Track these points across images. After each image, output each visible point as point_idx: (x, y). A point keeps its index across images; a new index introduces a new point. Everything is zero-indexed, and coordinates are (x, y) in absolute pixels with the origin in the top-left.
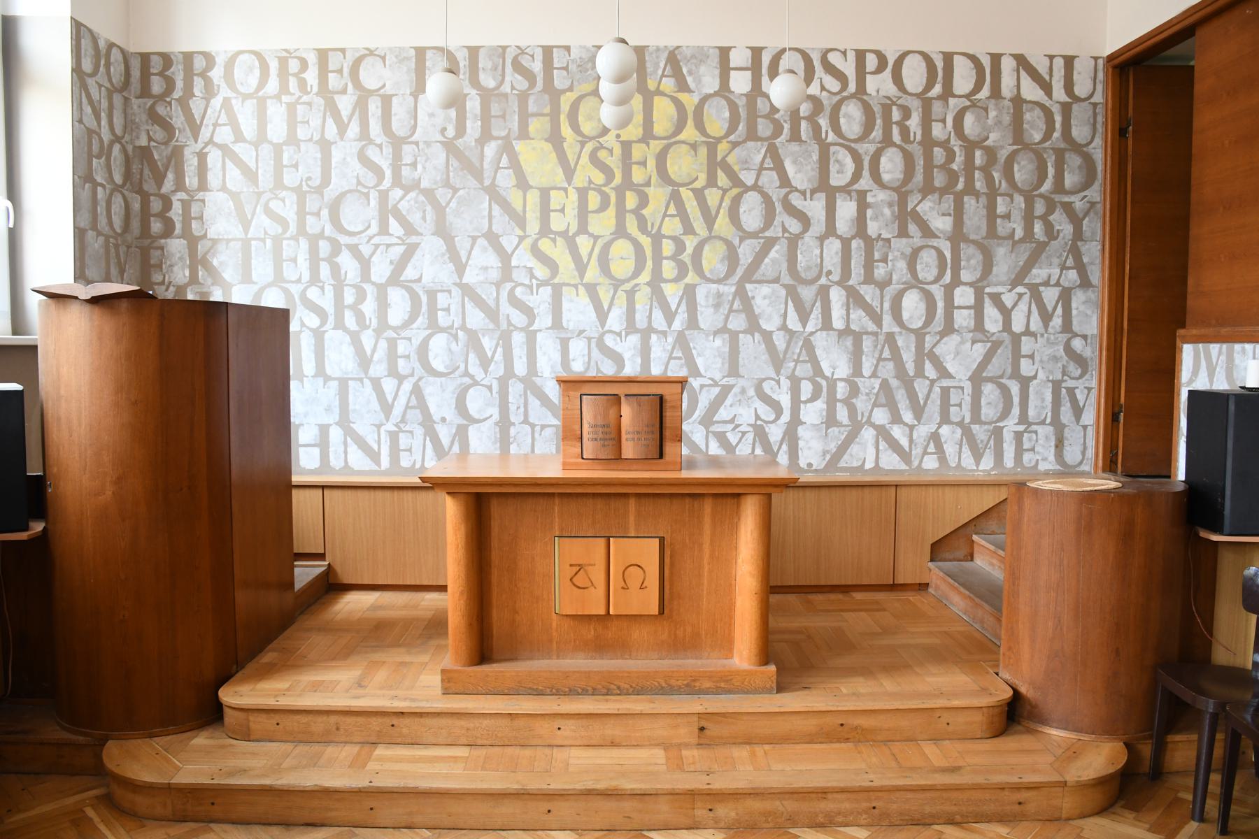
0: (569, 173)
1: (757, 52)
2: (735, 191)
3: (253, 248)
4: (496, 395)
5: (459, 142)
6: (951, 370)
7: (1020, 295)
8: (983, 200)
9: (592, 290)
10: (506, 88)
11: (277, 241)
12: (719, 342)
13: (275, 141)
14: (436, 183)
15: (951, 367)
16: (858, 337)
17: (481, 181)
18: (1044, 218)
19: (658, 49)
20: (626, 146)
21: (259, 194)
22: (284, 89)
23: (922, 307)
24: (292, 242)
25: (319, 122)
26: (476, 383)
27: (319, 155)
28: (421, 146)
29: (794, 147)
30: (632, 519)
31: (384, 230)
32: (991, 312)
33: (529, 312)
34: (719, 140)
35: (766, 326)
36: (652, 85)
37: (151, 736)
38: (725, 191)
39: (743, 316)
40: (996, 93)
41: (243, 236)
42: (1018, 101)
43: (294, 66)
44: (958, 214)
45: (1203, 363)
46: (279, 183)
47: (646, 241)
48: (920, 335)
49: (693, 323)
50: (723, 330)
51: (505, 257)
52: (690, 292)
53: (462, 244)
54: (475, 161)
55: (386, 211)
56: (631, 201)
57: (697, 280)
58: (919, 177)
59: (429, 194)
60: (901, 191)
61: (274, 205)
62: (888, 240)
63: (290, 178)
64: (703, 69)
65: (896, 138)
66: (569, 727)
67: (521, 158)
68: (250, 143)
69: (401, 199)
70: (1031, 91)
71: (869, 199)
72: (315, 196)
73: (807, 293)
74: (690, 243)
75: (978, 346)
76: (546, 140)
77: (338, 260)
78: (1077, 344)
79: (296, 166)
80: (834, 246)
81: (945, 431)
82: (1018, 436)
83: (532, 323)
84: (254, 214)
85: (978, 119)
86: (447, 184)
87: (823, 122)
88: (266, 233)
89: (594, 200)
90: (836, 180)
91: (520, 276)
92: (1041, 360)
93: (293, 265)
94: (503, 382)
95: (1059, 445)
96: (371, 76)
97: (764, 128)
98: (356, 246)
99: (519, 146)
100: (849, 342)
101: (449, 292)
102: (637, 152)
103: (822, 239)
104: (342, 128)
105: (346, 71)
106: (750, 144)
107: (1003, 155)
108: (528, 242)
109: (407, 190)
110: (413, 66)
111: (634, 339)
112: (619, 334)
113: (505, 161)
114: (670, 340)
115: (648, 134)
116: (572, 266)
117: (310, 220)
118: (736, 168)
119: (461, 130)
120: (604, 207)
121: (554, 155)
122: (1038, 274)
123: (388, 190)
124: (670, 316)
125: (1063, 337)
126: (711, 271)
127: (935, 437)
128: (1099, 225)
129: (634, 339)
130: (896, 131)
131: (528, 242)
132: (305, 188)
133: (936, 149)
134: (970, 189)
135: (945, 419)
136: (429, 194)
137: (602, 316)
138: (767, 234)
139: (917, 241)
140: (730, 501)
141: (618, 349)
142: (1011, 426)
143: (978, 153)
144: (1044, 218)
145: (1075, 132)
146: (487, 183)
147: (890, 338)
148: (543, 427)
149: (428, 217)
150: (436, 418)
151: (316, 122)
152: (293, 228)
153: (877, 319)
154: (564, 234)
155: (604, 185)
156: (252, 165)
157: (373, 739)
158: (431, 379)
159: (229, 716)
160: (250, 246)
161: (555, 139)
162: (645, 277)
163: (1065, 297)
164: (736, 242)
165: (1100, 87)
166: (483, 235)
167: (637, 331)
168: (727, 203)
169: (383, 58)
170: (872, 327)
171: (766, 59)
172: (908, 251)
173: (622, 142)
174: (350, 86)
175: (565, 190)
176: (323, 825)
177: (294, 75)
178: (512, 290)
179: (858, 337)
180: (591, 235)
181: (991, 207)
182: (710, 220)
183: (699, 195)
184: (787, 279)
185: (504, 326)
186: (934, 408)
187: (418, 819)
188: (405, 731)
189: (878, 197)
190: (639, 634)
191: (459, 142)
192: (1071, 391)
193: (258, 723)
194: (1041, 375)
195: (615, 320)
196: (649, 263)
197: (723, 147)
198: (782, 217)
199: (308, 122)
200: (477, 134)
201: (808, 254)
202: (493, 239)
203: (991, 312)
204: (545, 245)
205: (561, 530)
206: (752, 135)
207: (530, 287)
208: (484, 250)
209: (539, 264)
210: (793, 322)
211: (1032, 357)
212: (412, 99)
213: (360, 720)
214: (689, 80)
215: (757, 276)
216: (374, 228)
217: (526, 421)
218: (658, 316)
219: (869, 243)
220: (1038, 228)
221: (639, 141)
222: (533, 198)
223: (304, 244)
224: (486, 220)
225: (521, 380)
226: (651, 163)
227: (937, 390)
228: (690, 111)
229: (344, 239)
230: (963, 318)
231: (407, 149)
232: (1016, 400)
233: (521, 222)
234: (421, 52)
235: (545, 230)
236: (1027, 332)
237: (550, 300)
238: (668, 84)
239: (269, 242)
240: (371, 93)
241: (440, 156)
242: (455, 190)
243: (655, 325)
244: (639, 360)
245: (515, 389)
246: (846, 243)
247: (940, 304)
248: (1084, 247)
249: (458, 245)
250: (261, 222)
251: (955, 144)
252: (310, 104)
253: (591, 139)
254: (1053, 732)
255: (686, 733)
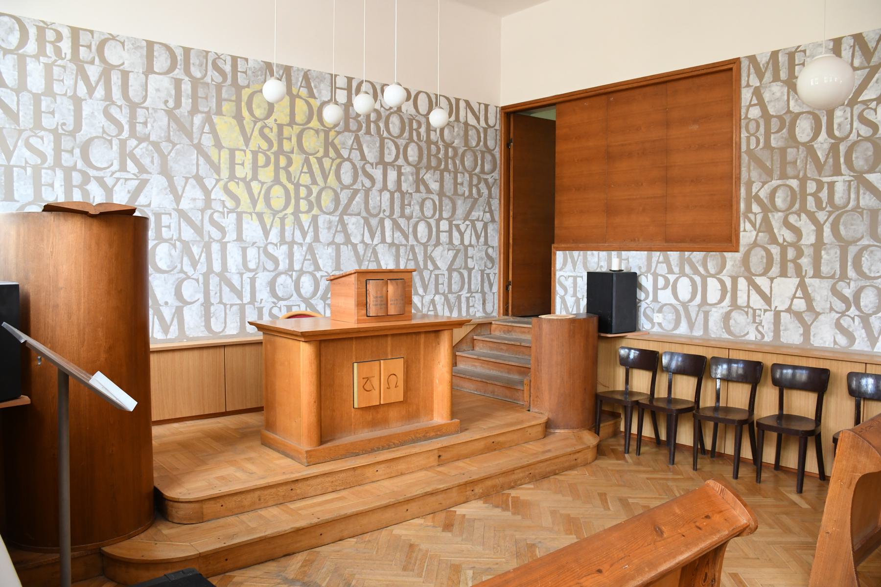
0: (247, 141)
1: (350, 80)
2: (338, 160)
3: (15, 174)
4: (201, 285)
5: (177, 112)
6: (439, 265)
7: (468, 225)
8: (452, 174)
9: (260, 216)
10: (208, 79)
11: (37, 170)
12: (330, 250)
13: (34, 91)
14: (160, 138)
15: (439, 264)
16: (398, 247)
17: (191, 139)
18: (477, 186)
19: (298, 70)
20: (280, 127)
21: (21, 132)
22: (42, 51)
23: (426, 230)
24: (49, 172)
25: (72, 82)
26: (188, 277)
27: (72, 107)
28: (150, 111)
29: (368, 137)
30: (389, 349)
31: (123, 168)
32: (456, 234)
33: (222, 230)
34: (330, 129)
35: (354, 241)
36: (295, 91)
37: (130, 537)
38: (333, 160)
39: (343, 234)
40: (457, 119)
41: (5, 163)
42: (466, 124)
43: (50, 35)
44: (442, 181)
45: (569, 260)
46: (38, 125)
47: (291, 187)
48: (425, 245)
49: (316, 239)
50: (332, 243)
51: (207, 192)
52: (315, 219)
53: (179, 182)
54: (188, 125)
55: (124, 155)
56: (283, 162)
57: (319, 212)
58: (425, 160)
59: (156, 145)
60: (417, 167)
61: (33, 141)
62: (411, 194)
63: (47, 122)
64: (322, 85)
65: (415, 138)
66: (382, 469)
67: (218, 128)
68: (12, 89)
69: (136, 147)
70: (472, 121)
71: (403, 171)
72: (69, 138)
73: (374, 222)
74: (315, 190)
75: (450, 252)
76: (234, 117)
77: (88, 187)
78: (490, 251)
79: (53, 113)
80: (386, 196)
81: (437, 298)
82: (468, 299)
83: (224, 237)
84: (15, 146)
85: (450, 132)
86: (168, 140)
87: (382, 125)
88: (26, 162)
89: (261, 159)
90: (388, 158)
91: (217, 206)
92: (476, 259)
93: (50, 189)
94: (206, 276)
95: (484, 304)
96: (113, 55)
97: (353, 126)
98: (102, 178)
99: (216, 119)
100: (394, 250)
101: (170, 214)
102: (287, 131)
103: (381, 191)
104: (91, 90)
105: (94, 48)
106: (346, 133)
107: (460, 151)
108: (222, 183)
109: (141, 140)
110: (145, 53)
111: (285, 248)
112: (276, 245)
113: (207, 128)
114: (305, 248)
115: (292, 122)
116: (249, 201)
117: (65, 156)
118: (339, 147)
119: (178, 103)
120: (267, 164)
121: (237, 128)
122: (475, 215)
123: (126, 139)
124: (304, 234)
125: (485, 247)
126: (326, 207)
127: (433, 301)
128: (498, 191)
129: (285, 248)
130: (415, 133)
131: (222, 183)
132: (60, 131)
133: (432, 146)
134: (446, 169)
135: (437, 292)
136: (156, 145)
137: (266, 233)
138: (355, 187)
139: (424, 195)
140: (433, 335)
141: (275, 254)
142: (464, 294)
143: (450, 150)
144: (477, 186)
145: (489, 143)
146: (195, 141)
147: (412, 247)
148: (232, 305)
149: (155, 161)
150: (161, 302)
151: (69, 82)
152: (50, 160)
153: (406, 237)
154: (244, 180)
155: (268, 150)
156: (14, 107)
157: (281, 501)
158: (158, 275)
159: (181, 512)
160: (12, 172)
161: (239, 117)
162: (290, 209)
163: (485, 227)
164: (339, 191)
165: (498, 122)
166: (193, 177)
167: (286, 243)
168: (334, 167)
169: (123, 44)
170: (404, 242)
171: (354, 85)
172: (420, 200)
173: (278, 125)
174: (97, 59)
175: (244, 151)
176: (294, 553)
177: (50, 42)
178: (212, 214)
179: (398, 247)
180: (260, 181)
181: (455, 178)
182: (325, 177)
183: (319, 160)
184: (364, 214)
185: (206, 239)
186: (432, 286)
187: (345, 534)
188: (298, 491)
189: (407, 169)
190: (393, 413)
191: (177, 112)
192: (488, 275)
193: (208, 508)
194: (476, 267)
195: (274, 236)
196: (293, 201)
197: (332, 134)
198: (361, 177)
199: (62, 81)
200: (189, 108)
201: (374, 199)
202: (199, 179)
203: (456, 234)
204: (232, 186)
205: (356, 358)
206: (347, 129)
207: (223, 213)
208: (194, 187)
209: (229, 199)
210: (368, 240)
211: (472, 258)
212: (143, 76)
213: (273, 490)
214: (315, 91)
215: (349, 211)
216: (116, 166)
217: (221, 302)
218: (298, 233)
219: (403, 194)
220: (474, 191)
221: (287, 125)
222: (225, 154)
223: (60, 174)
224: (195, 167)
225: (218, 275)
226: (294, 139)
227: (433, 276)
228: (315, 110)
229: (92, 173)
230: (444, 237)
231: (140, 112)
232: (466, 280)
233: (217, 169)
234: (150, 45)
235: (232, 177)
236: (471, 245)
237: (235, 222)
238: (304, 92)
239: (29, 170)
240: (114, 67)
241: (163, 120)
242: (174, 145)
243: (296, 239)
244: (287, 261)
245: (214, 281)
246: (392, 194)
247: (434, 230)
248: (492, 202)
249: (176, 183)
250: (22, 154)
251: (440, 143)
252: (64, 67)
253: (260, 120)
254: (557, 431)
255: (433, 460)
